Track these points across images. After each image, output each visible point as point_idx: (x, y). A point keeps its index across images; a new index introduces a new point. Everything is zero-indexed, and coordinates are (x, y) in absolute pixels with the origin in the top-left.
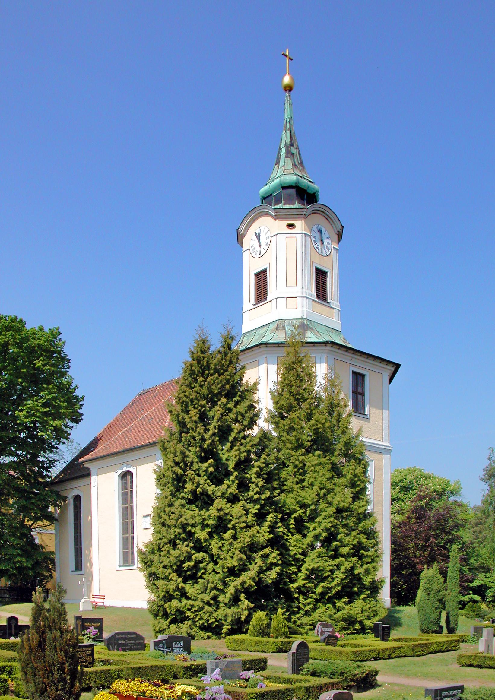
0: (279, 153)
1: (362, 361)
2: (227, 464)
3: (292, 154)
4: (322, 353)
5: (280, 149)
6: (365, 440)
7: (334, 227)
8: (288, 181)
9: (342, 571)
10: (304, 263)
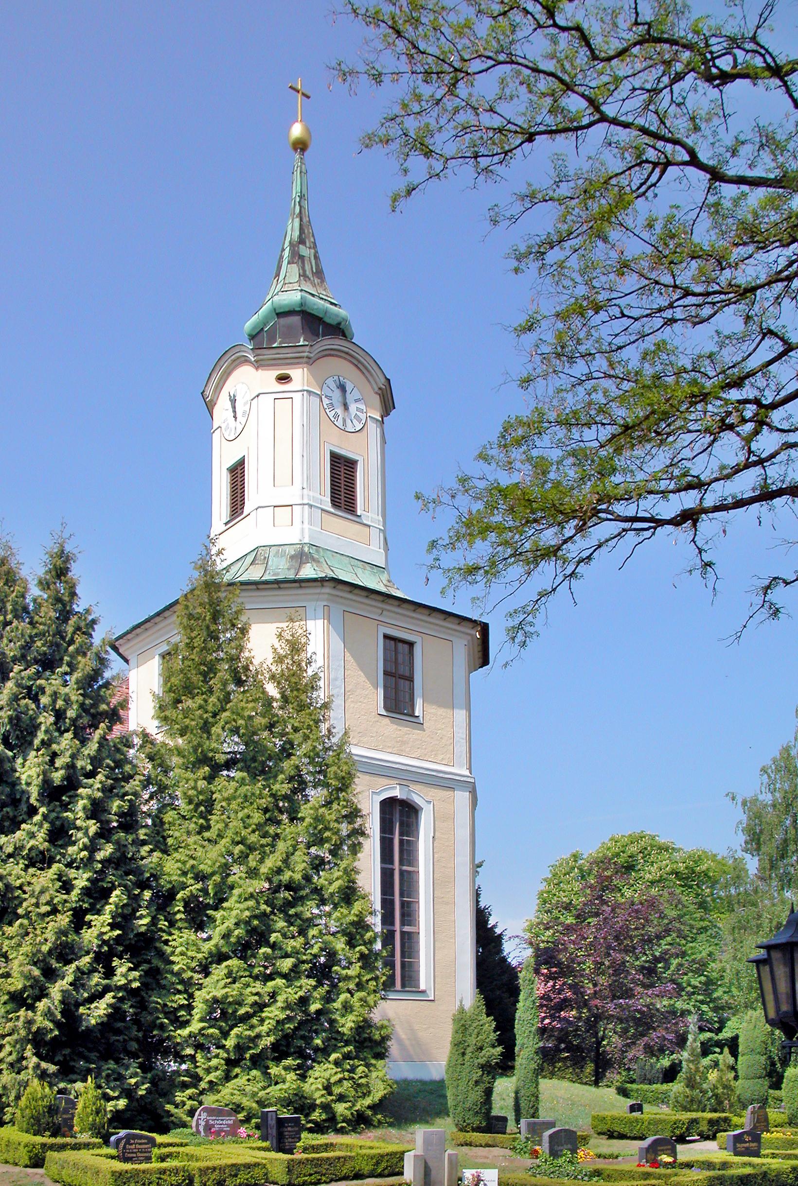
0: (281, 257)
1: (405, 615)
2: (28, 792)
3: (302, 258)
5: (283, 250)
6: (355, 750)
7: (373, 382)
8: (286, 302)
9: (280, 1004)
10: (307, 443)
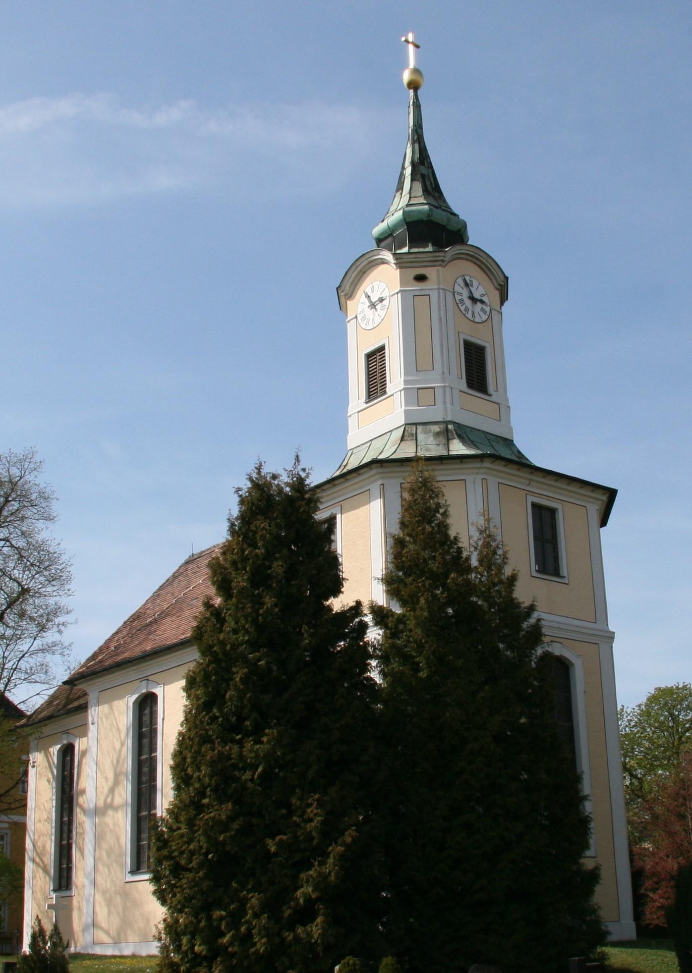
0: (402, 176)
4: (477, 473)
